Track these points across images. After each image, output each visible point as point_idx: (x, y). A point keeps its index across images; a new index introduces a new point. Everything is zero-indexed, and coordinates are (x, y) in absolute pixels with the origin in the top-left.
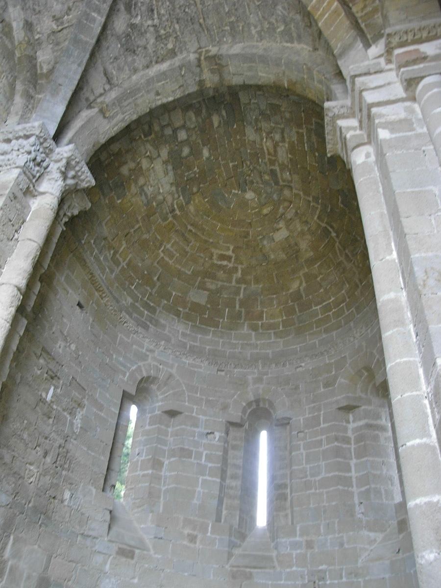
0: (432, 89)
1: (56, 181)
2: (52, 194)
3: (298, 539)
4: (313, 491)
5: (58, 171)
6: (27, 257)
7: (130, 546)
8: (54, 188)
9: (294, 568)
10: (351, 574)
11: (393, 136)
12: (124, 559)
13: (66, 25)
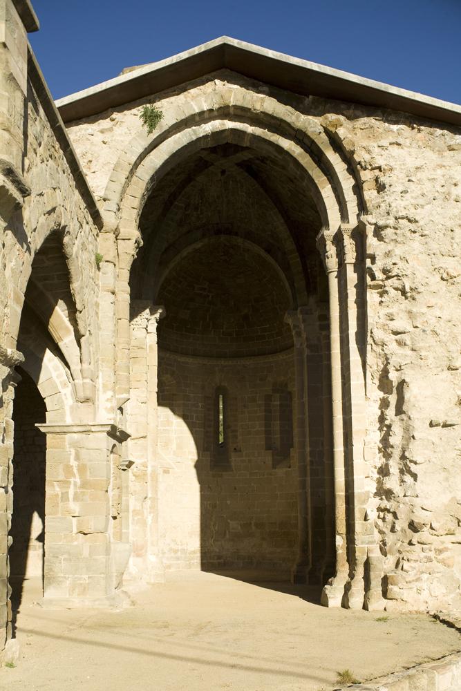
3: (244, 458)
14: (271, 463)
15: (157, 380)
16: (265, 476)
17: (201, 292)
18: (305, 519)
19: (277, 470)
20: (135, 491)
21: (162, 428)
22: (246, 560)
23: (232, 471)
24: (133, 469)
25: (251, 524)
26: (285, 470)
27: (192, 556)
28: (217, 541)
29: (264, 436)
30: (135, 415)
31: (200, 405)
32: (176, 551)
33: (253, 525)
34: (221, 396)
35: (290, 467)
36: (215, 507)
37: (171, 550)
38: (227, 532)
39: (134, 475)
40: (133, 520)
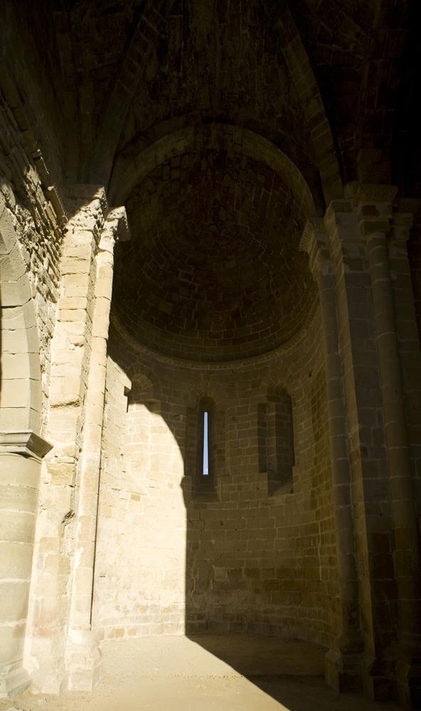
0: (362, 418)
3: (233, 485)
4: (242, 456)
5: (112, 230)
6: (106, 313)
7: (137, 493)
9: (230, 501)
10: (263, 504)
11: (352, 272)
12: (135, 501)
13: (106, 63)
14: (266, 488)
15: (108, 322)
16: (260, 507)
17: (186, 280)
18: (352, 563)
19: (274, 498)
20: (49, 501)
21: (134, 444)
22: (234, 621)
23: (219, 501)
24: (49, 460)
25: (241, 570)
26: (285, 496)
27: (165, 614)
28: (199, 594)
29: (257, 454)
30: (63, 364)
31: (181, 417)
32: (144, 609)
33: (243, 571)
34: (206, 414)
35: (292, 492)
36: (197, 548)
37: (138, 606)
38: (56, 227)
39: (51, 472)
40: (41, 557)
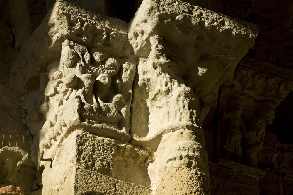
1: (168, 91)
2: (173, 130)
5: (159, 70)
8: (172, 110)
